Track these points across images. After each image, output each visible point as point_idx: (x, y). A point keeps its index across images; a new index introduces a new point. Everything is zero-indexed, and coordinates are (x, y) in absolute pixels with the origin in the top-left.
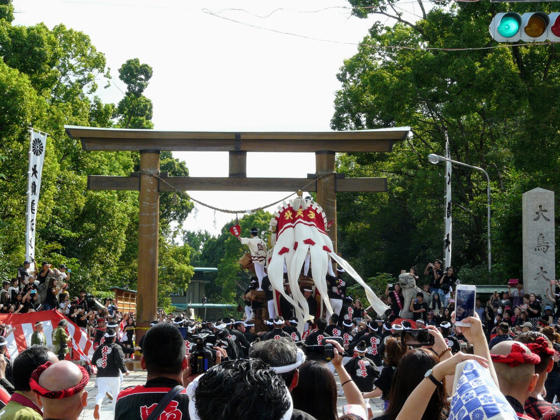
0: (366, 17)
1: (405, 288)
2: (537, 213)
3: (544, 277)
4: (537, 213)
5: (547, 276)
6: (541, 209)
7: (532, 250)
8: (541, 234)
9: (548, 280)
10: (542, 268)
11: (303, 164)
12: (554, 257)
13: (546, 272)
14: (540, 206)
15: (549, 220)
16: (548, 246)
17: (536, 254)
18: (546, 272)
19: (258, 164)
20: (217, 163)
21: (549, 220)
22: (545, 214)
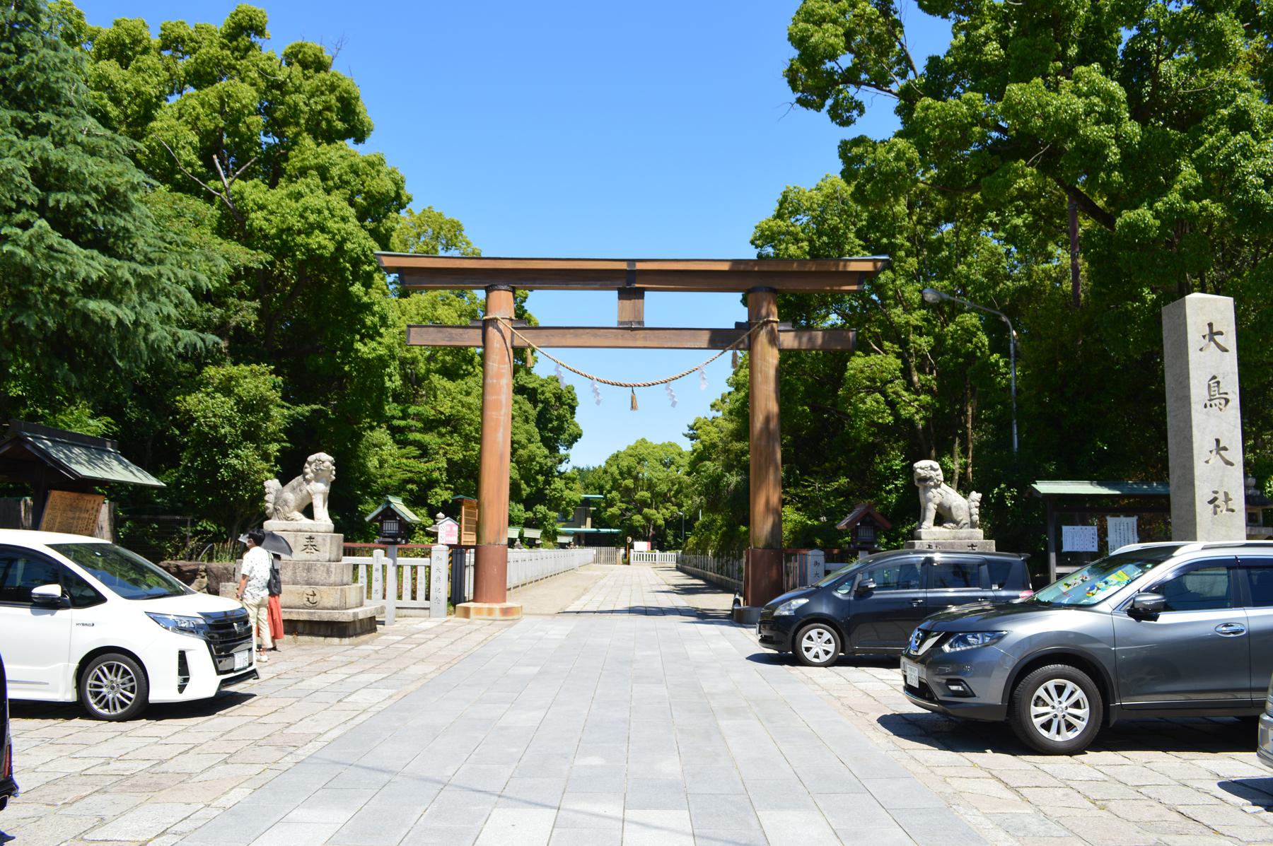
18: (1225, 449)
19: (661, 307)
20: (602, 306)
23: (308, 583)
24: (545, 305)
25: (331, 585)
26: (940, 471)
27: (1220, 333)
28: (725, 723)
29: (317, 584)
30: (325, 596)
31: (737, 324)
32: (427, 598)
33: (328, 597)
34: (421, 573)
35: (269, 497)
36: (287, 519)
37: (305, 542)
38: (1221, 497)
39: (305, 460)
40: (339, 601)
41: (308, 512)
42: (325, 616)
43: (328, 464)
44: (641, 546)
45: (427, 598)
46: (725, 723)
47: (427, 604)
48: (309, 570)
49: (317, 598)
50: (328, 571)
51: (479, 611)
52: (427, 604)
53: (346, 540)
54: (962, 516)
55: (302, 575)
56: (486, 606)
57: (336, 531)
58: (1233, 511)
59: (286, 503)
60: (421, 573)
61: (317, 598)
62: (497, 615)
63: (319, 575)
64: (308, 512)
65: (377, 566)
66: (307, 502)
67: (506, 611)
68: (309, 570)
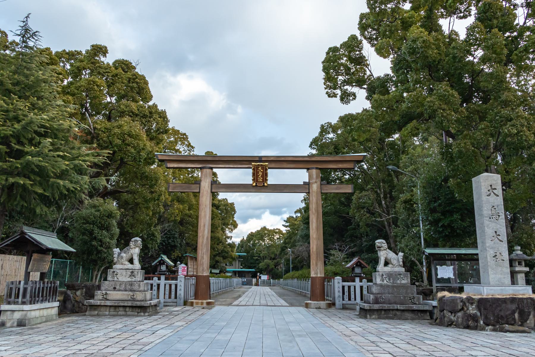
0: (92, 46)
1: (380, 250)
2: (489, 190)
3: (494, 193)
4: (489, 190)
5: (500, 238)
6: (492, 188)
7: (488, 219)
8: (493, 207)
9: (501, 241)
10: (491, 186)
11: (300, 176)
12: (505, 224)
13: (499, 235)
14: (491, 186)
15: (498, 196)
16: (499, 216)
17: (490, 221)
18: (499, 235)
19: (275, 176)
20: (244, 176)
21: (498, 196)
22: (500, 238)
23: (131, 291)
24: (225, 175)
25: (140, 291)
26: (386, 244)
27: (495, 189)
28: (297, 339)
29: (135, 291)
30: (138, 296)
31: (304, 182)
32: (176, 297)
33: (139, 296)
34: (173, 287)
35: (116, 256)
36: (122, 264)
37: (130, 274)
38: (498, 254)
39: (130, 241)
40: (144, 295)
41: (131, 261)
42: (138, 304)
43: (140, 242)
44: (264, 277)
45: (176, 297)
46: (297, 339)
47: (175, 300)
48: (131, 285)
49: (135, 297)
50: (139, 286)
51: (197, 303)
52: (175, 300)
53: (146, 274)
54: (395, 262)
55: (128, 287)
56: (200, 301)
57: (142, 269)
58: (503, 260)
59: (122, 257)
60: (173, 287)
61: (135, 297)
62: (205, 305)
63: (136, 287)
64: (131, 261)
65: (155, 284)
66: (130, 257)
67: (208, 304)
68: (131, 285)
